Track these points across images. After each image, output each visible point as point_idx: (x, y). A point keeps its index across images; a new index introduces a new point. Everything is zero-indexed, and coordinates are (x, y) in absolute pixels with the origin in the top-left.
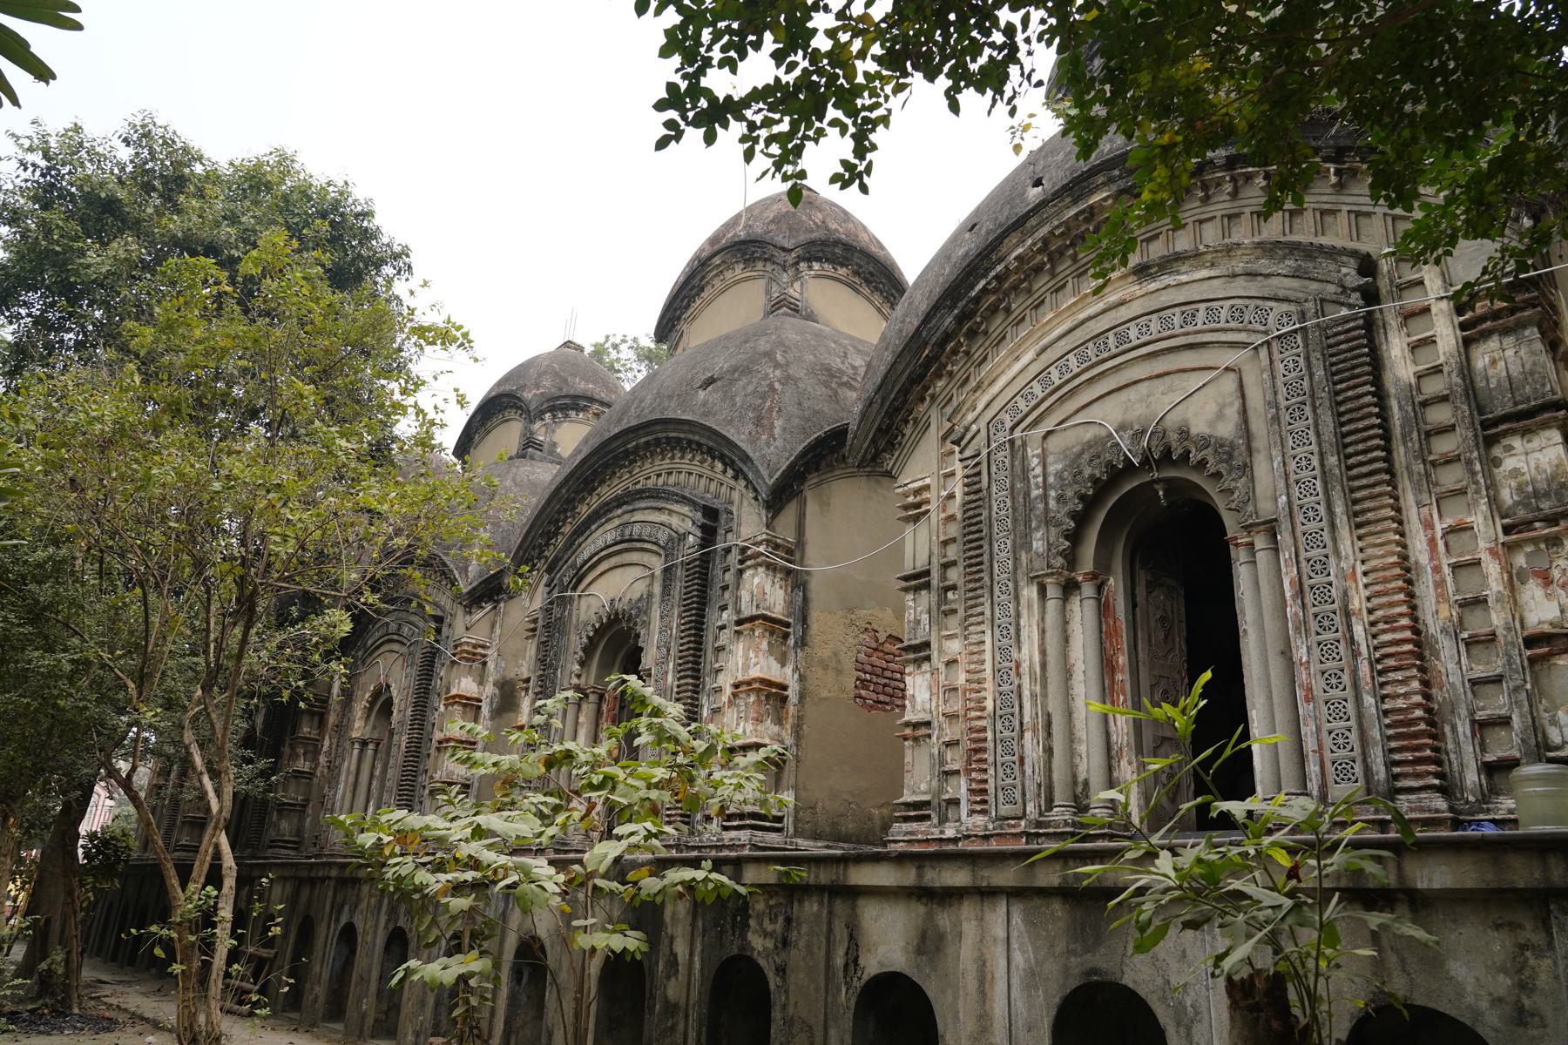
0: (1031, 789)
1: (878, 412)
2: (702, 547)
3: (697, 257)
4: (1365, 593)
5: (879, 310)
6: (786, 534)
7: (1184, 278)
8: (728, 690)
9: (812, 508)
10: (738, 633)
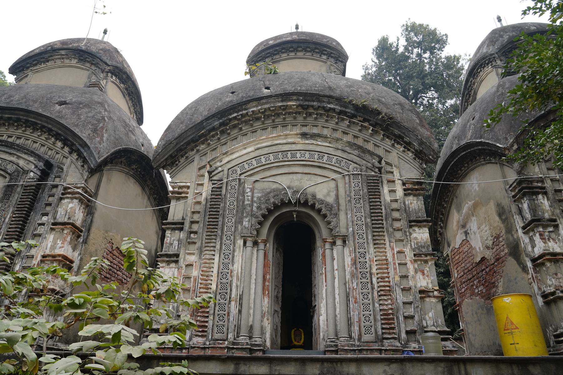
1: (173, 148)
2: (39, 180)
3: (49, 45)
4: (376, 267)
5: (129, 108)
6: (92, 187)
7: (320, 143)
8: (39, 258)
9: (104, 179)
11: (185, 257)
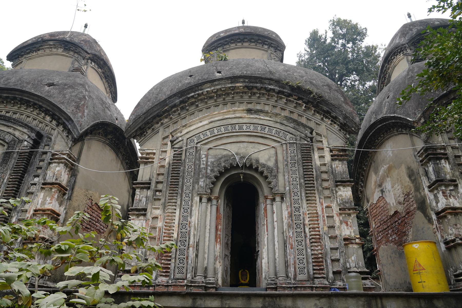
0: (190, 269)
1: (142, 121)
2: (32, 148)
4: (308, 219)
5: (106, 89)
6: (75, 154)
7: (262, 117)
8: (32, 212)
9: (85, 147)
10: (42, 188)
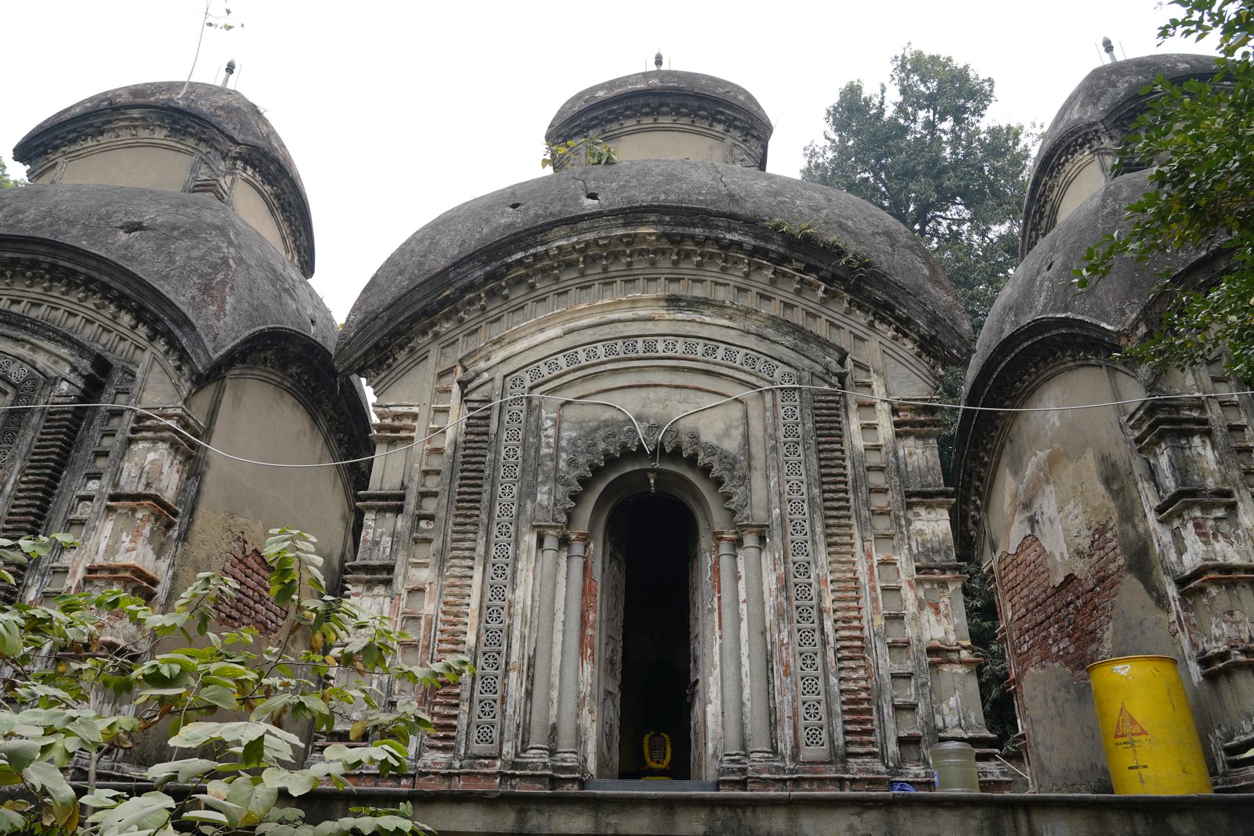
1: (381, 329)
2: (80, 400)
4: (832, 597)
5: (284, 239)
6: (199, 416)
7: (708, 319)
8: (81, 573)
9: (227, 398)
10: (110, 509)
11: (406, 572)
